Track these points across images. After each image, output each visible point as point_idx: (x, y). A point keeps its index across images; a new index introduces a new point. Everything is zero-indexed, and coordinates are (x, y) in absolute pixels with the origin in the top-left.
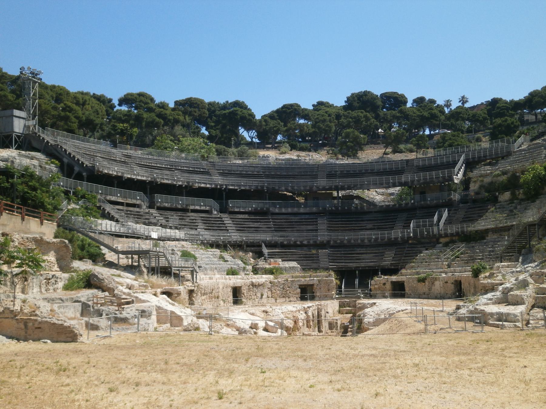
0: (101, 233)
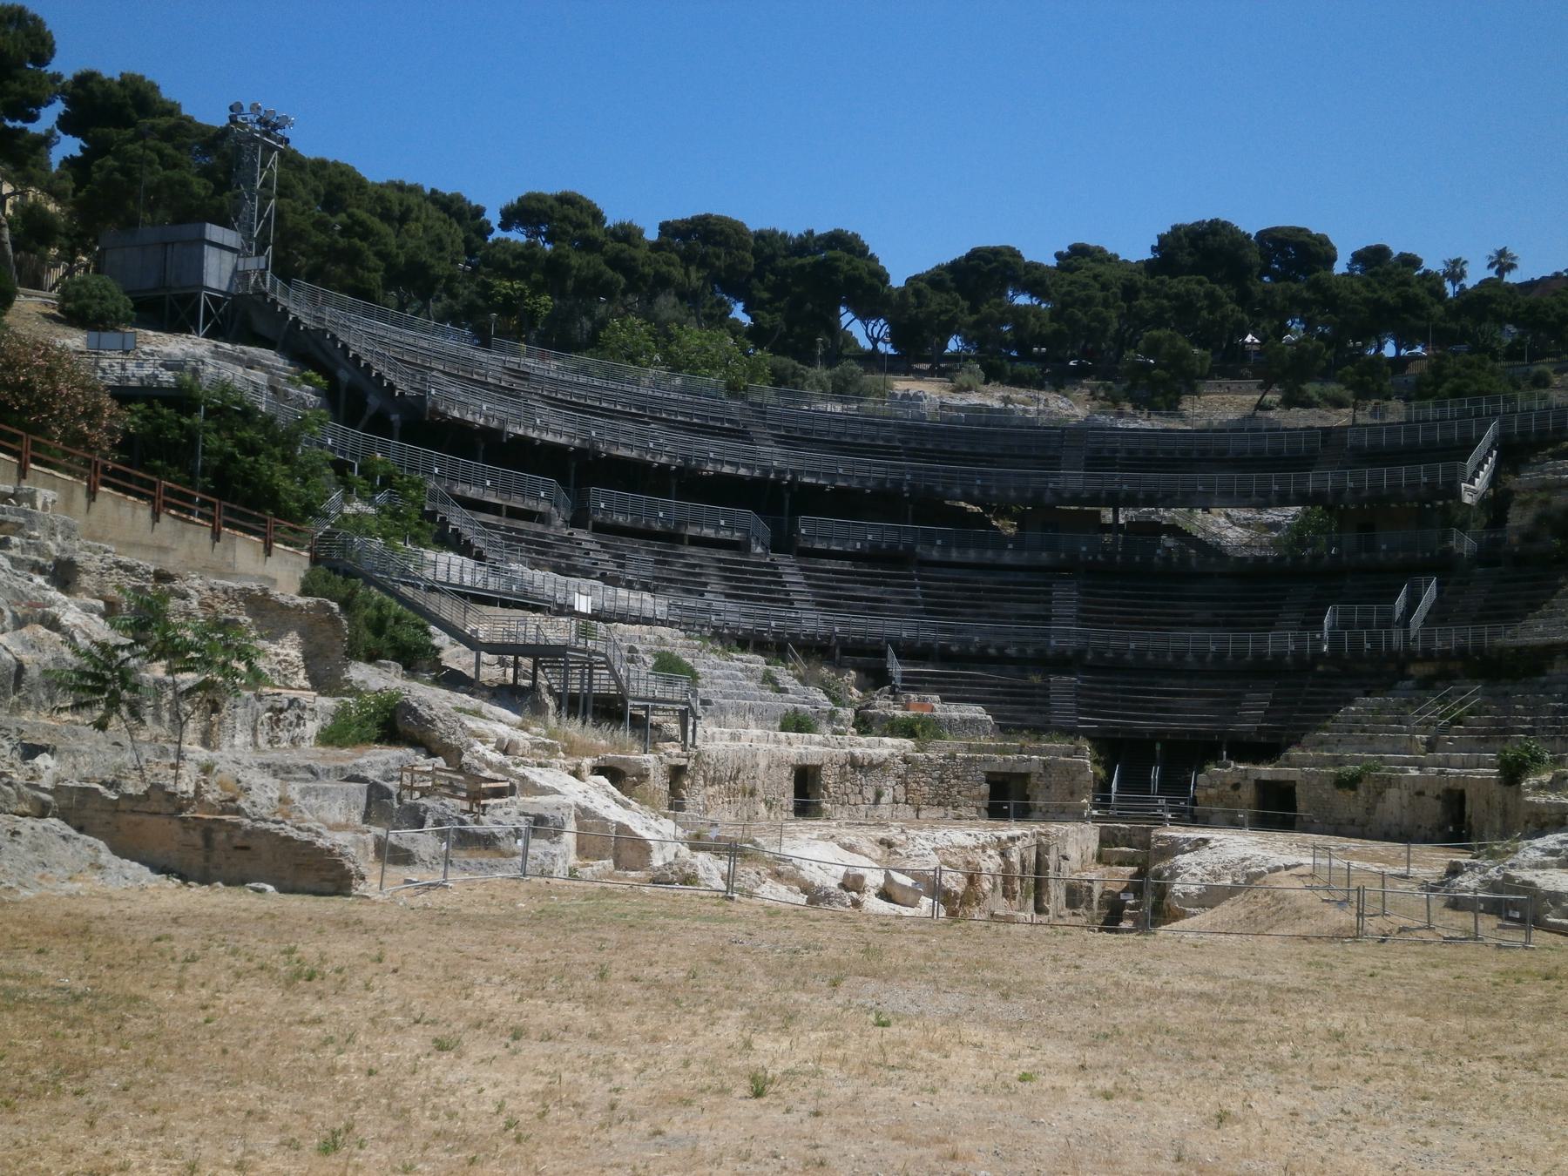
0: (431, 589)
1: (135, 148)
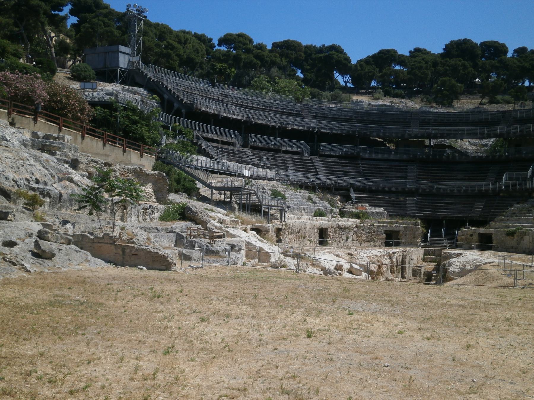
0: (196, 169)
1: (95, 20)
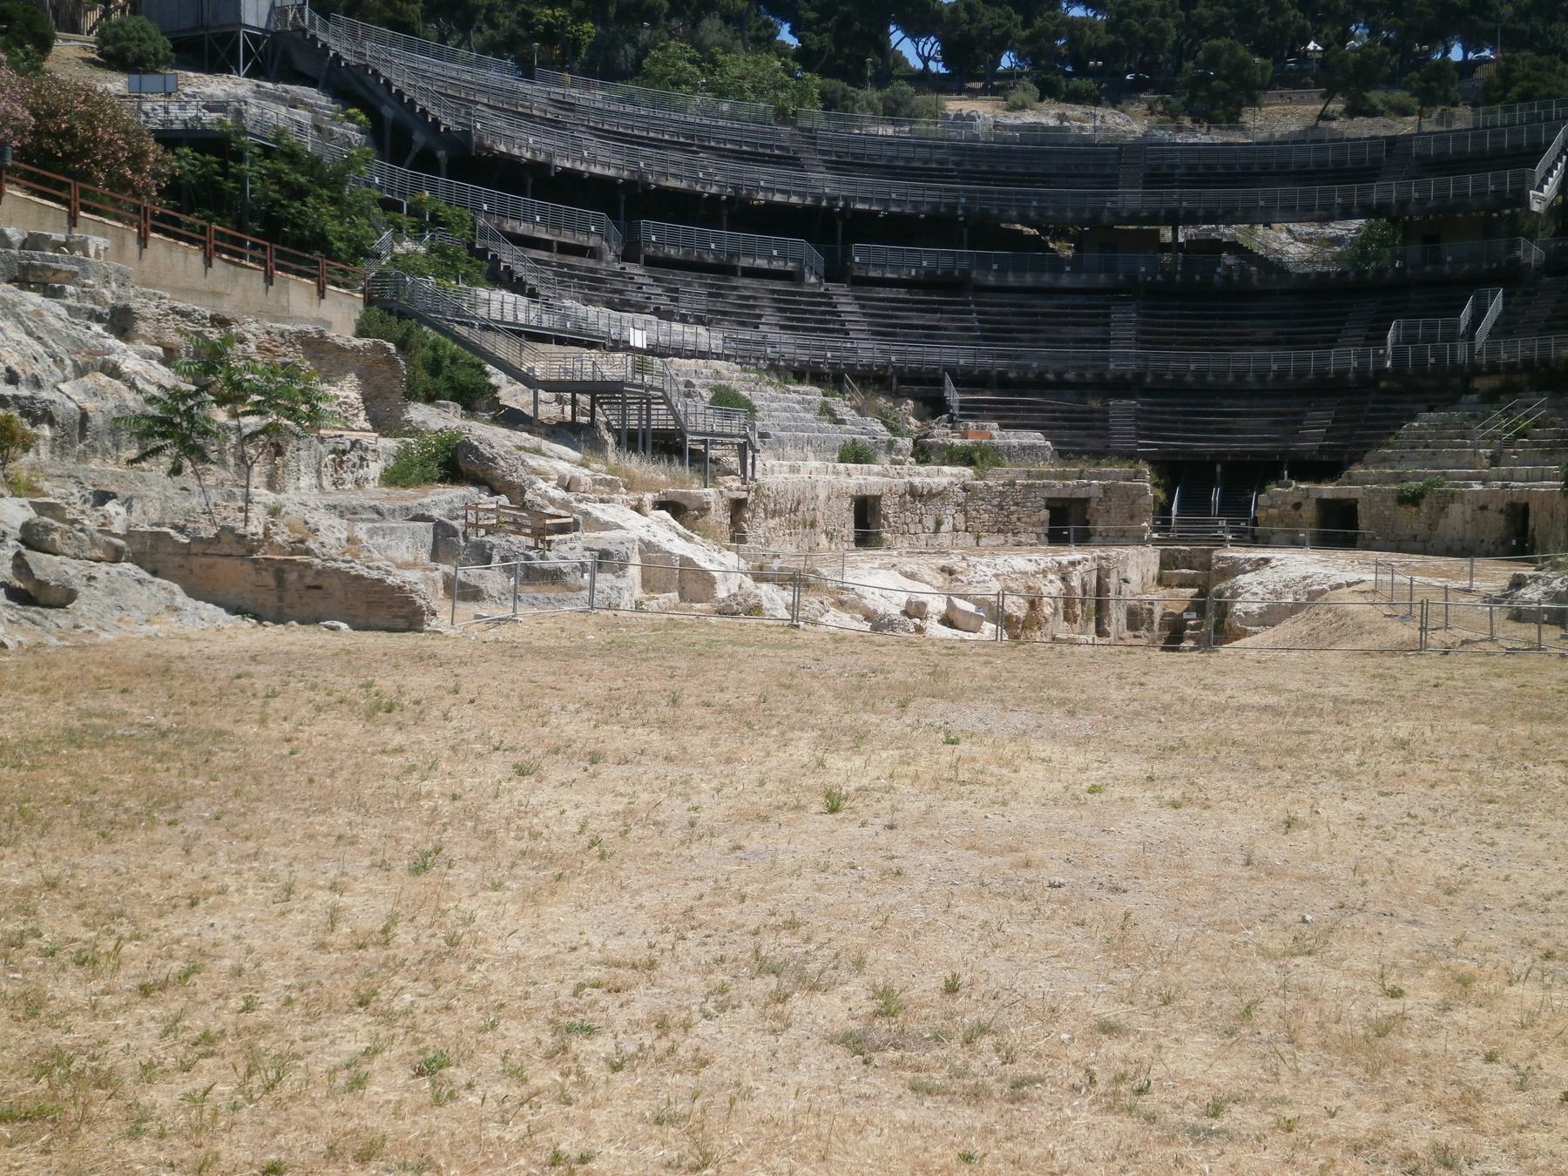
0: (486, 328)
